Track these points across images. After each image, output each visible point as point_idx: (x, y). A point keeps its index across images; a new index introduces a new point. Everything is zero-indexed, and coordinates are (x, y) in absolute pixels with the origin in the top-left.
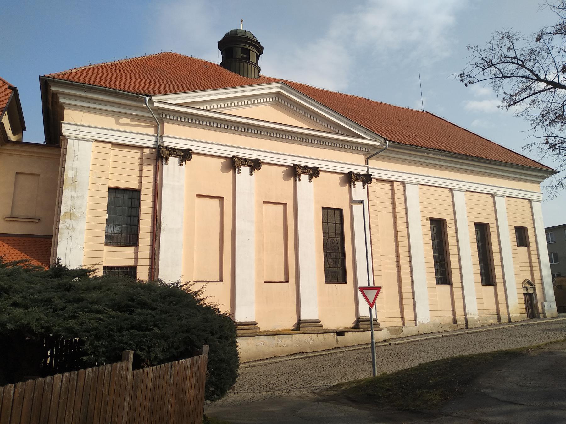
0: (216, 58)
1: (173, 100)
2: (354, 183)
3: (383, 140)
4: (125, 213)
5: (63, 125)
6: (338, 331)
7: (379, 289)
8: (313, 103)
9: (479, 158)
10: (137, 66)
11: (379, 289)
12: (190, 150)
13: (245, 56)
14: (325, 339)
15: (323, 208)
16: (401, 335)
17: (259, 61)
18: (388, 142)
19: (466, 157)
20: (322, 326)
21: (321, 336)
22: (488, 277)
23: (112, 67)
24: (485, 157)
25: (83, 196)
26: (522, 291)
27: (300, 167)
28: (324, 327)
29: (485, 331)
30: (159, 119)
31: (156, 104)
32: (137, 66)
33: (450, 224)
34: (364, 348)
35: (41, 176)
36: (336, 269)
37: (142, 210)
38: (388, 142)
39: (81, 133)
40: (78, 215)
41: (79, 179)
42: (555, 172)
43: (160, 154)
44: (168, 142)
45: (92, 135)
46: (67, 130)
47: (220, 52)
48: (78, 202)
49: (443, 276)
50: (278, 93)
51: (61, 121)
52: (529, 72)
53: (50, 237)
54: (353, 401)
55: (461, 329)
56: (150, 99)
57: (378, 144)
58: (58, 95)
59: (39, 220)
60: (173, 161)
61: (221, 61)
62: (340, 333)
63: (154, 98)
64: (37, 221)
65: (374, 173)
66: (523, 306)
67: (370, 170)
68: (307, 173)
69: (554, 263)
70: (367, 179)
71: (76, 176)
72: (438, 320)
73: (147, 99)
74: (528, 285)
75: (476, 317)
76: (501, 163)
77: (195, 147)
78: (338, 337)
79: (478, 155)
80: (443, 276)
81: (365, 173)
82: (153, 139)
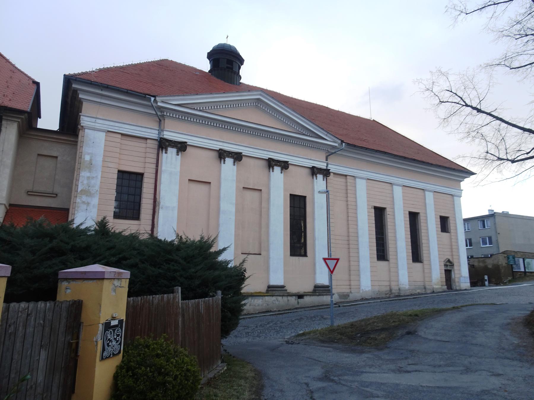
0: (205, 66)
1: (173, 102)
2: (316, 175)
3: (340, 142)
4: (130, 191)
5: (81, 117)
6: (299, 294)
7: (338, 260)
8: (286, 108)
9: (414, 160)
10: (141, 70)
11: (338, 260)
12: (186, 142)
13: (229, 66)
14: (288, 300)
15: (290, 195)
16: (348, 300)
17: (240, 71)
18: (344, 144)
19: (405, 158)
20: (286, 290)
21: (285, 298)
22: (416, 256)
23: (122, 70)
24: (419, 159)
25: (97, 177)
26: (443, 268)
27: (317, 169)
28: (288, 291)
29: (413, 297)
30: (161, 116)
31: (159, 104)
32: (141, 70)
33: (388, 211)
34: (320, 309)
35: (59, 158)
36: (298, 244)
37: (144, 190)
38: (344, 144)
39: (97, 125)
40: (93, 192)
41: (93, 163)
42: (473, 174)
43: (163, 144)
44: (168, 135)
45: (105, 126)
46: (85, 121)
47: (208, 61)
48: (93, 182)
49: (382, 253)
50: (258, 99)
51: (80, 114)
52: (460, 99)
53: (68, 210)
54: (323, 341)
55: (395, 297)
56: (155, 100)
57: (336, 145)
58: (78, 92)
59: (57, 195)
60: (172, 151)
61: (209, 69)
62: (300, 296)
63: (157, 99)
64: (55, 196)
65: (333, 168)
66: (444, 280)
67: (329, 166)
68: (279, 166)
69: (468, 247)
70: (326, 173)
71: (91, 160)
72: (377, 289)
73: (153, 99)
74: (448, 264)
75: (407, 287)
76: (431, 165)
77: (244, 151)
78: (299, 300)
79: (414, 158)
80: (382, 253)
81: (325, 168)
82: (157, 132)
